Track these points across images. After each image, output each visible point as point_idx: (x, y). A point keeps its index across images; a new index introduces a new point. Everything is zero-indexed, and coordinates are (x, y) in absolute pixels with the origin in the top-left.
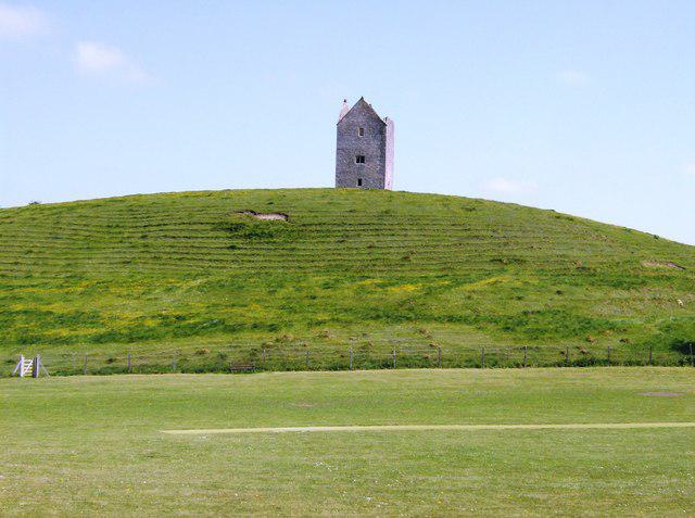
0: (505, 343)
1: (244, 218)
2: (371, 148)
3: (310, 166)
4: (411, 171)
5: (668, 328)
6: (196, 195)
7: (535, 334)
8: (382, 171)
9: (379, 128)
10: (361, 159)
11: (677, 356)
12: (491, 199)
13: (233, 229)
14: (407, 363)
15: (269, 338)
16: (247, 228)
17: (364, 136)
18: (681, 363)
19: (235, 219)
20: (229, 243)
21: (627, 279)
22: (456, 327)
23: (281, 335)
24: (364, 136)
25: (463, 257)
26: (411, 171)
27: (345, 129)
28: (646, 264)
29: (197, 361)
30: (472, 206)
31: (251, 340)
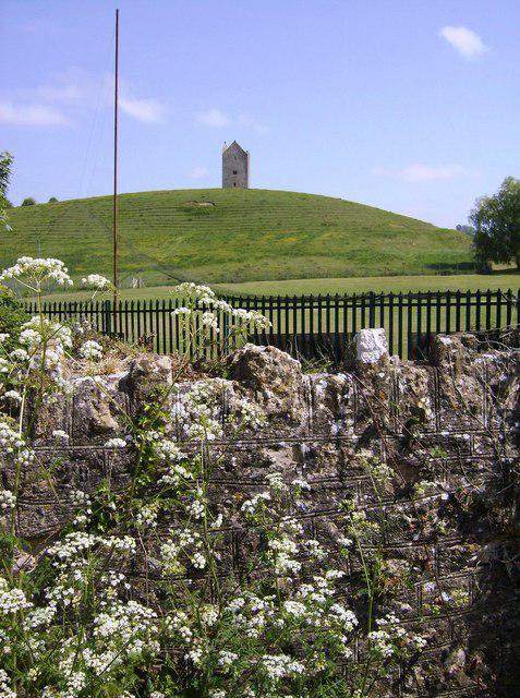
0: (351, 266)
1: (191, 205)
2: (240, 167)
3: (206, 176)
4: (260, 178)
5: (419, 257)
6: (162, 193)
7: (364, 261)
8: (246, 179)
9: (244, 156)
10: (235, 173)
11: (427, 271)
12: (221, 172)
13: (188, 210)
14: (312, 276)
15: (241, 266)
16: (190, 209)
17: (236, 161)
18: (436, 274)
19: (187, 205)
20: (186, 218)
21: (388, 235)
22: (325, 258)
23: (245, 263)
24: (236, 161)
25: (307, 223)
26: (260, 178)
27: (227, 157)
28: (392, 226)
29: (388, 272)
30: (304, 197)
31: (233, 267)
